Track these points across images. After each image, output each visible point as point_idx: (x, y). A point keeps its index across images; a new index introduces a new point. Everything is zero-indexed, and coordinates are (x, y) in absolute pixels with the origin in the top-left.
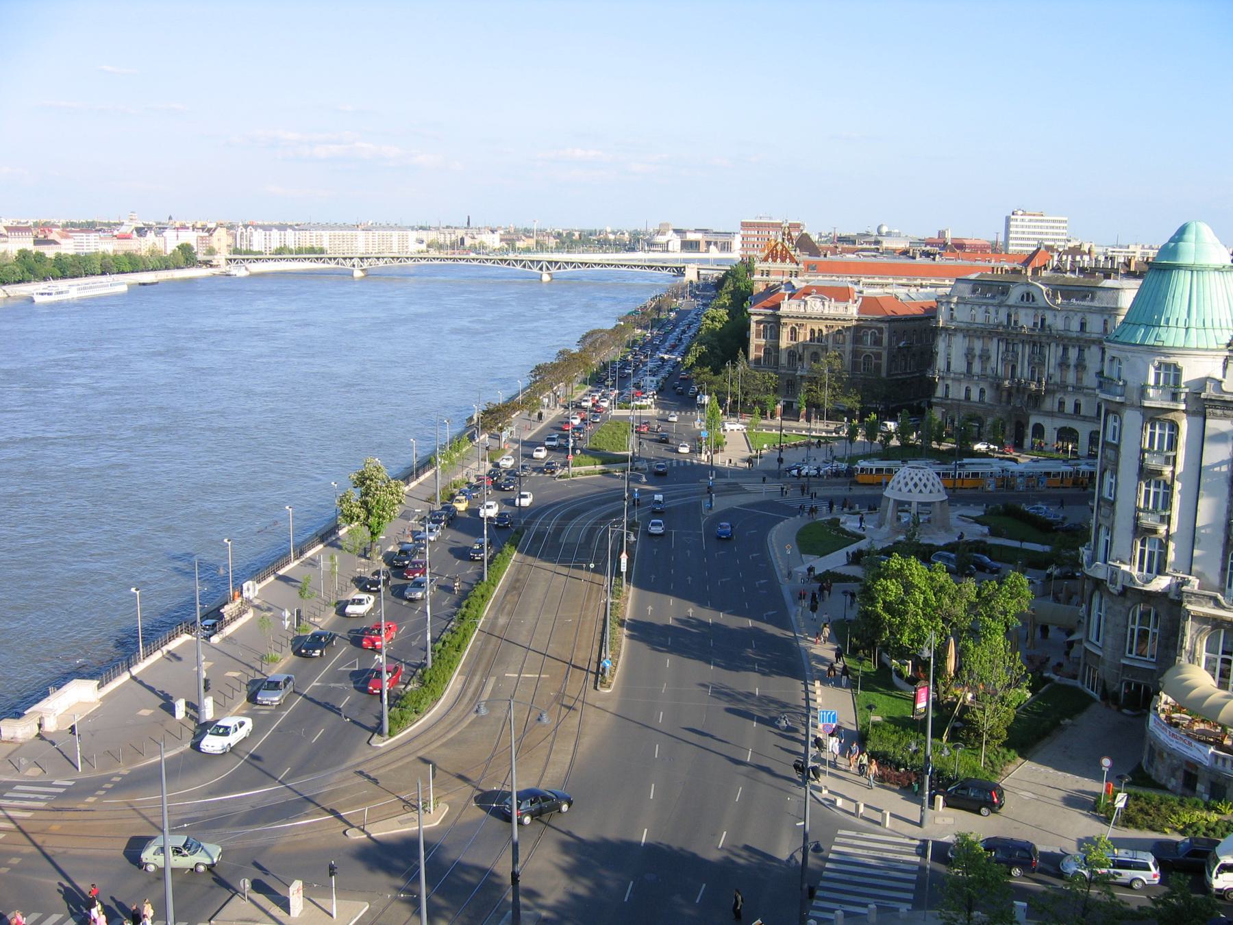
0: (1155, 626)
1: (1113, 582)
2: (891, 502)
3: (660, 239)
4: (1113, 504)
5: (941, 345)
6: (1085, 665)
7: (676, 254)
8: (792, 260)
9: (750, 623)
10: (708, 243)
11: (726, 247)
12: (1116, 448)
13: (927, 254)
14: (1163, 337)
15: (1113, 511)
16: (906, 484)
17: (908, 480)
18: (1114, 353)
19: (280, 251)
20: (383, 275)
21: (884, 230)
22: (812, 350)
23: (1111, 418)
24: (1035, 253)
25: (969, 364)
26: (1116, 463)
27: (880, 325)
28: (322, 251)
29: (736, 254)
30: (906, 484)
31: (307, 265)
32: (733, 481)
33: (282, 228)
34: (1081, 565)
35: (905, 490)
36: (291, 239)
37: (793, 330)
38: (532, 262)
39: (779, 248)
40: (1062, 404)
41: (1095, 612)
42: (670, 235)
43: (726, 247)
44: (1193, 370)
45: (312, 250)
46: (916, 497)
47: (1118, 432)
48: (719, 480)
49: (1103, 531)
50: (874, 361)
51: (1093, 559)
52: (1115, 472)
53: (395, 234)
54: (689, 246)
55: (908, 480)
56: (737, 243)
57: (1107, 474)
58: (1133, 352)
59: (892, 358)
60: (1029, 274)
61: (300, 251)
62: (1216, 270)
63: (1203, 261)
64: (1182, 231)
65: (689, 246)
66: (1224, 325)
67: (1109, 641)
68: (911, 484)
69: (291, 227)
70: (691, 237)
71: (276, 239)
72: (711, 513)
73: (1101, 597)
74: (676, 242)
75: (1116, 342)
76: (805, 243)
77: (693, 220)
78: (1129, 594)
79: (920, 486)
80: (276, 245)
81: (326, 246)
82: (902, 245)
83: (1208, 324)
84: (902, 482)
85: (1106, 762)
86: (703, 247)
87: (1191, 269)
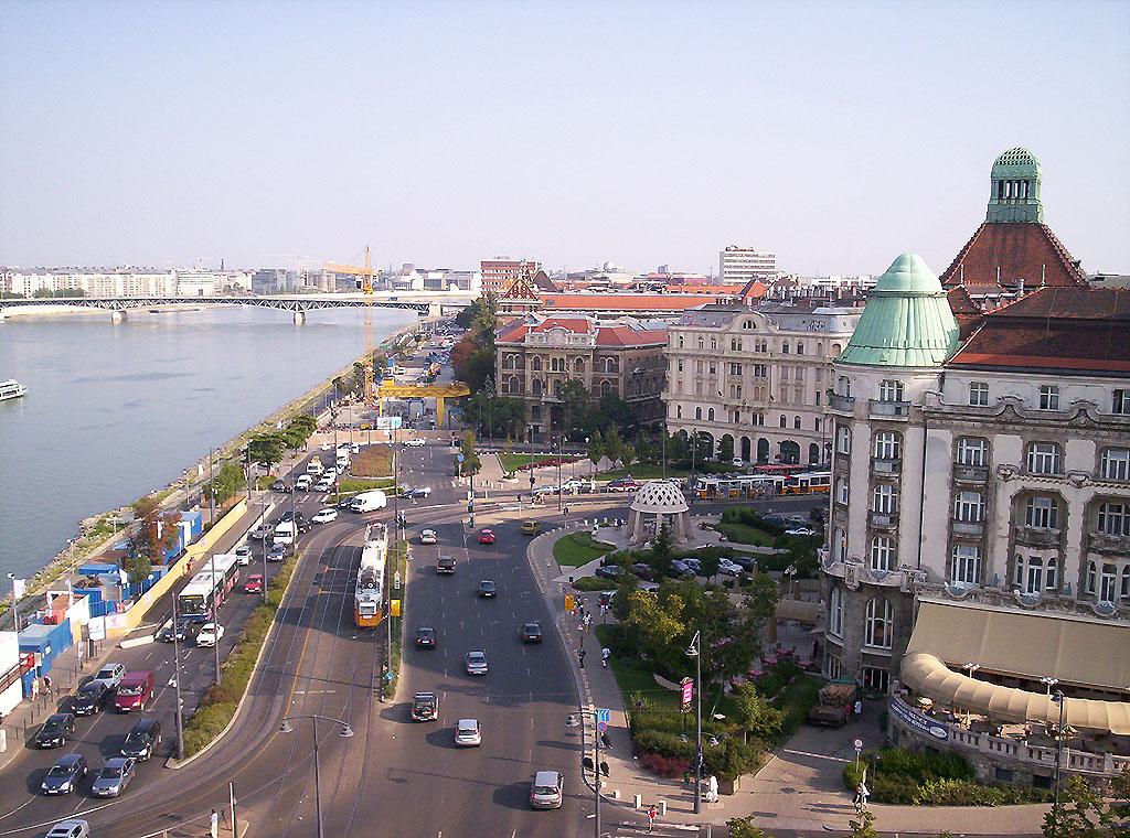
0: (890, 618)
1: (851, 578)
2: (638, 514)
3: (406, 279)
4: (846, 508)
5: (672, 372)
6: (828, 655)
7: (418, 294)
8: (532, 296)
9: (253, 674)
10: (449, 282)
11: (465, 285)
12: (848, 458)
13: (654, 288)
14: (886, 356)
15: (847, 515)
16: (651, 498)
17: (652, 493)
18: (843, 373)
19: (39, 294)
20: (695, 283)
21: (610, 266)
22: (554, 378)
23: (842, 430)
24: (750, 285)
25: (799, 378)
26: (848, 472)
27: (616, 353)
28: (81, 293)
29: (475, 292)
30: (651, 498)
31: (67, 308)
32: (491, 500)
33: (41, 271)
34: (820, 565)
35: (650, 503)
36: (50, 282)
37: (537, 360)
38: (270, 301)
39: (520, 284)
40: (783, 420)
41: (835, 607)
42: (414, 274)
43: (465, 285)
44: (913, 387)
45: (70, 293)
46: (661, 510)
47: (849, 444)
48: (478, 500)
49: (839, 534)
50: (612, 386)
51: (831, 559)
52: (847, 481)
53: (153, 277)
54: (433, 285)
55: (652, 493)
56: (476, 281)
57: (841, 482)
58: (861, 371)
59: (628, 383)
60: (750, 304)
61: (59, 294)
62: (930, 296)
63: (920, 289)
64: (899, 262)
65: (433, 285)
66: (939, 346)
67: (849, 631)
68: (656, 497)
69: (49, 271)
70: (432, 276)
71: (36, 283)
72: (473, 531)
73: (840, 592)
74: (419, 282)
75: (845, 363)
76: (543, 280)
77: (433, 261)
78: (865, 590)
79: (665, 499)
80: (35, 287)
81: (85, 287)
82: (627, 280)
83: (925, 345)
84: (647, 496)
85: (858, 743)
86: (444, 286)
87: (910, 296)
